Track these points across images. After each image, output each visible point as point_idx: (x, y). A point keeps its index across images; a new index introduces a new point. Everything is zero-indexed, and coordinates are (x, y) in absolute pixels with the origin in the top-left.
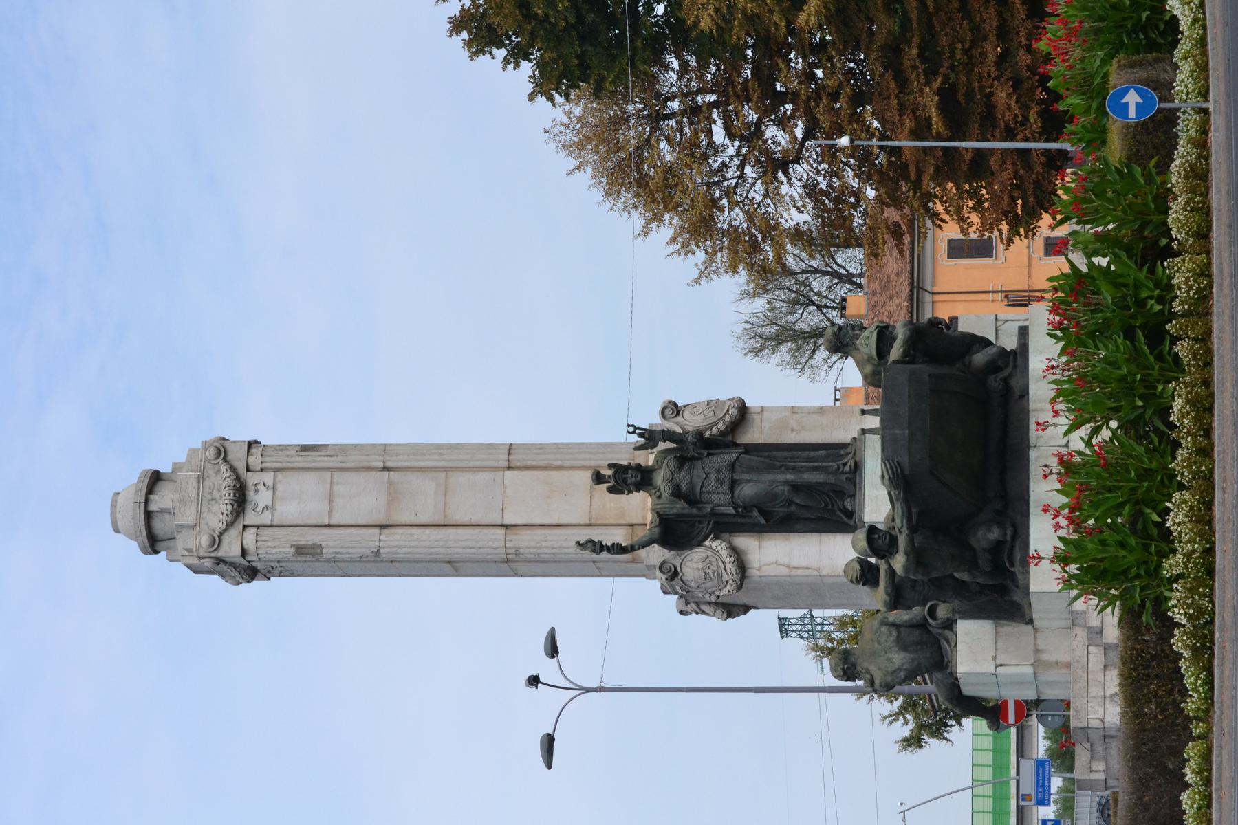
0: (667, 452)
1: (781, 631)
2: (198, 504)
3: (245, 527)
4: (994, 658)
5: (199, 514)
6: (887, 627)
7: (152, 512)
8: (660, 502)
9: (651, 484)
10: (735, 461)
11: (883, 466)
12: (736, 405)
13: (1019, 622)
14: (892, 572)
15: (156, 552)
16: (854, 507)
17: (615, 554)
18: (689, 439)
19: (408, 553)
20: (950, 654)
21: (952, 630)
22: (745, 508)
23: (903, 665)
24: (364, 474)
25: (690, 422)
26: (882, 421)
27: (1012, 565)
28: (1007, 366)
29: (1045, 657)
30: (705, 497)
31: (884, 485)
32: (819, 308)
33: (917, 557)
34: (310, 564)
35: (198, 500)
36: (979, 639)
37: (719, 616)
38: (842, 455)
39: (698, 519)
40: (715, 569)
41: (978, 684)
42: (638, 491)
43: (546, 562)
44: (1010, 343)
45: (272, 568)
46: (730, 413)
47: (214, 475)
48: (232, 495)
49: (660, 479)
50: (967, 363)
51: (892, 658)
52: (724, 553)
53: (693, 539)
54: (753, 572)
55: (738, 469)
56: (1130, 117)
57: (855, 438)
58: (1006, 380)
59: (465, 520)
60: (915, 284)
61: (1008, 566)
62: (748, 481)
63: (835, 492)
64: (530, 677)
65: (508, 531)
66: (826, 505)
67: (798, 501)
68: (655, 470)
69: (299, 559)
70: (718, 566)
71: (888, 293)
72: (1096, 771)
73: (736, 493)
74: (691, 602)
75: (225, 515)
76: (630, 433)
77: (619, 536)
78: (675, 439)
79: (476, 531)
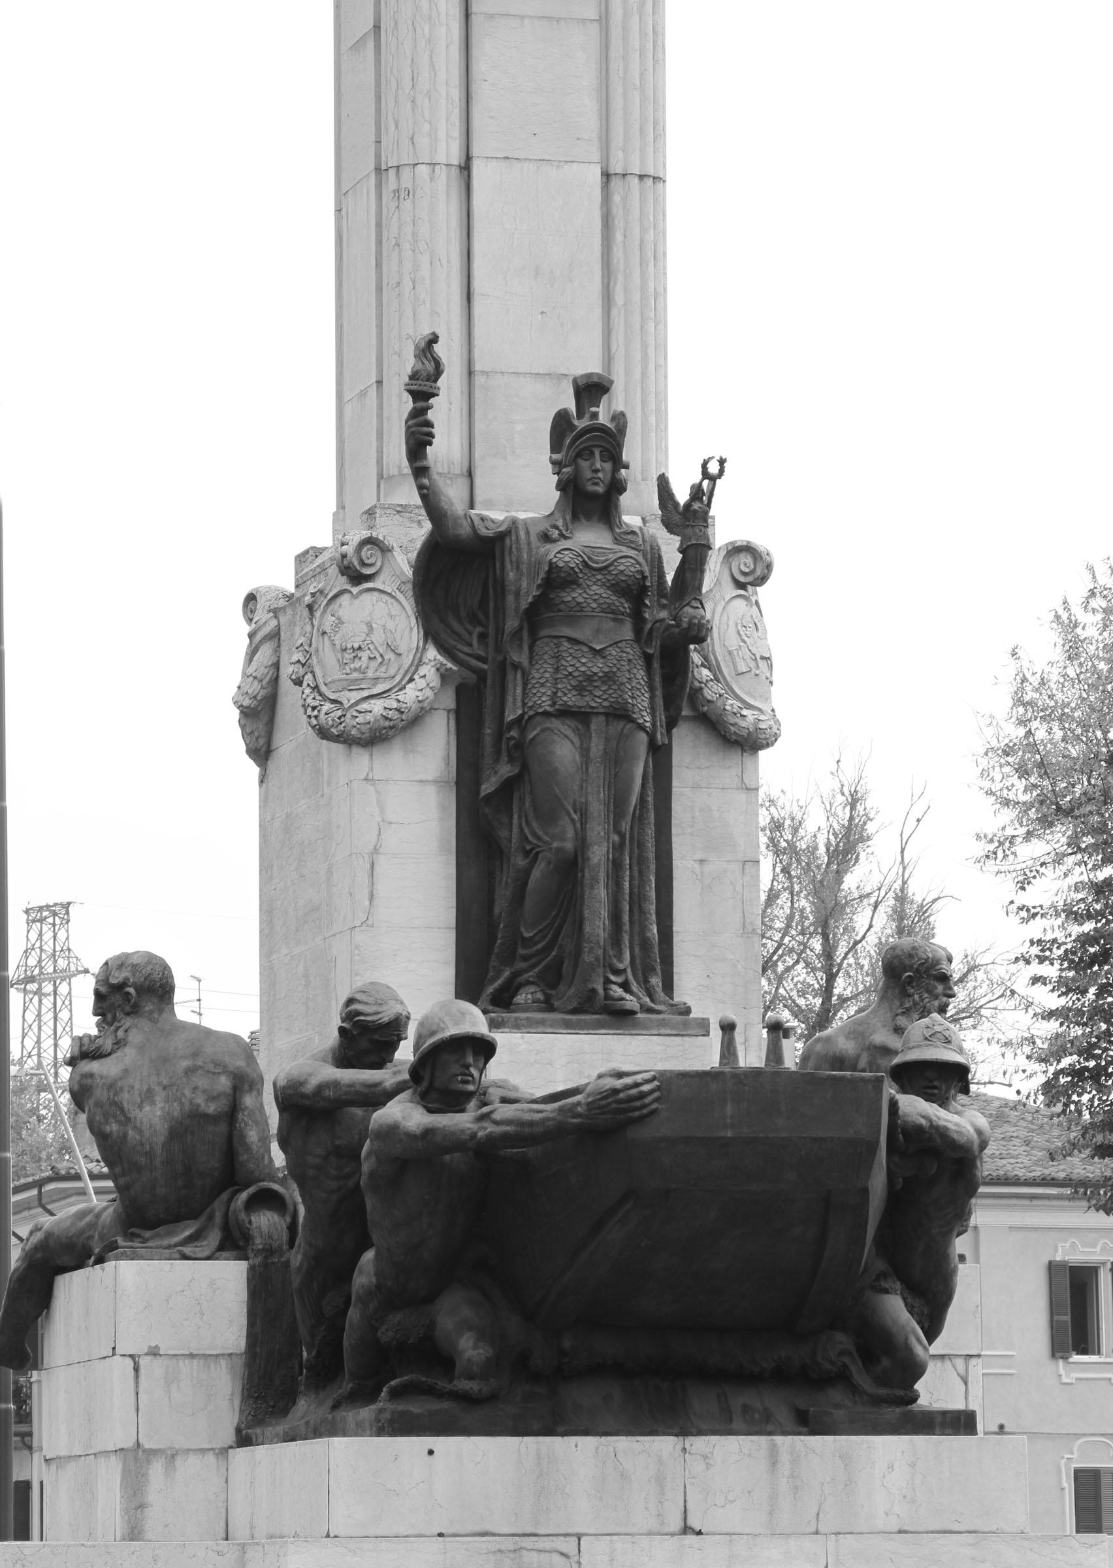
0: (656, 561)
1: (41, 909)
4: (154, 1352)
6: (229, 1091)
8: (534, 539)
9: (575, 517)
10: (633, 721)
11: (647, 1076)
12: (762, 726)
13: (241, 1411)
14: (377, 1097)
18: (688, 609)
20: (165, 1242)
21: (221, 1248)
23: (135, 1128)
26: (756, 1073)
27: (395, 1394)
28: (881, 1381)
29: (156, 1470)
30: (545, 648)
31: (600, 1077)
36: (202, 1314)
37: (245, 689)
38: (646, 981)
39: (491, 632)
40: (370, 674)
42: (562, 486)
43: (379, 265)
50: (884, 1284)
51: (153, 1103)
52: (410, 695)
53: (443, 621)
55: (617, 727)
57: (687, 1011)
58: (842, 1378)
59: (480, 67)
61: (393, 1383)
62: (585, 752)
63: (559, 963)
65: (455, 172)
66: (527, 942)
67: (536, 874)
68: (611, 529)
73: (555, 723)
76: (704, 465)
78: (688, 575)
79: (456, 94)
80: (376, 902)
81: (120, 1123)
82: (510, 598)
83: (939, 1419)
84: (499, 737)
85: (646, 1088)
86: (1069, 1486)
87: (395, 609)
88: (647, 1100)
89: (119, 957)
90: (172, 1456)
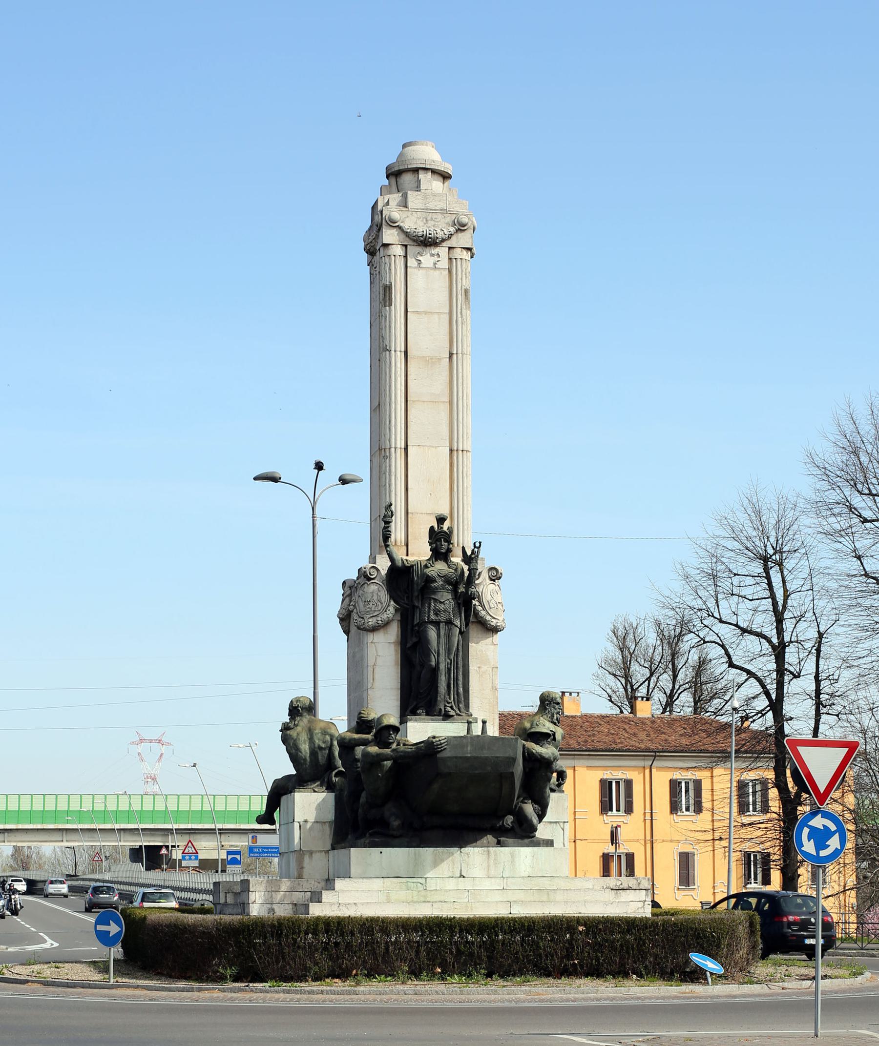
2: (424, 209)
3: (406, 246)
5: (416, 210)
7: (418, 174)
10: (454, 624)
11: (443, 738)
12: (498, 624)
15: (388, 177)
16: (420, 715)
17: (383, 532)
19: (385, 373)
22: (418, 632)
24: (447, 338)
25: (484, 587)
26: (478, 736)
27: (371, 835)
29: (306, 859)
32: (649, 679)
33: (374, 762)
34: (378, 297)
35: (427, 209)
38: (458, 706)
41: (288, 808)
44: (542, 831)
45: (375, 268)
46: (493, 620)
47: (446, 221)
48: (430, 236)
49: (440, 567)
54: (370, 637)
56: (97, 926)
57: (472, 715)
60: (658, 754)
61: (370, 832)
64: (322, 463)
67: (423, 672)
69: (381, 288)
70: (375, 611)
71: (652, 733)
72: (226, 896)
74: (351, 589)
75: (414, 230)
76: (475, 544)
77: (397, 533)
80: (375, 680)
81: (296, 750)
82: (415, 586)
83: (542, 842)
84: (412, 630)
85: (442, 742)
86: (677, 859)
87: (381, 589)
88: (443, 745)
89: (296, 698)
90: (311, 853)
